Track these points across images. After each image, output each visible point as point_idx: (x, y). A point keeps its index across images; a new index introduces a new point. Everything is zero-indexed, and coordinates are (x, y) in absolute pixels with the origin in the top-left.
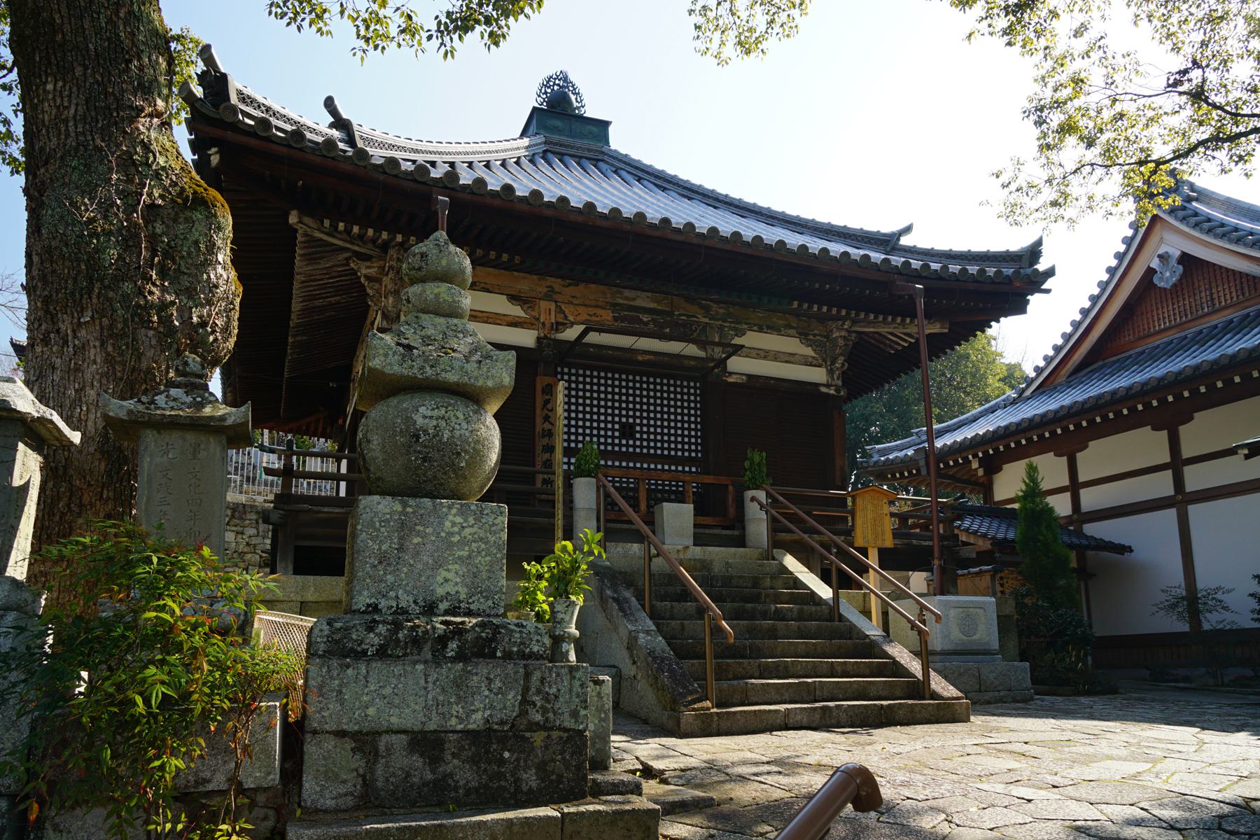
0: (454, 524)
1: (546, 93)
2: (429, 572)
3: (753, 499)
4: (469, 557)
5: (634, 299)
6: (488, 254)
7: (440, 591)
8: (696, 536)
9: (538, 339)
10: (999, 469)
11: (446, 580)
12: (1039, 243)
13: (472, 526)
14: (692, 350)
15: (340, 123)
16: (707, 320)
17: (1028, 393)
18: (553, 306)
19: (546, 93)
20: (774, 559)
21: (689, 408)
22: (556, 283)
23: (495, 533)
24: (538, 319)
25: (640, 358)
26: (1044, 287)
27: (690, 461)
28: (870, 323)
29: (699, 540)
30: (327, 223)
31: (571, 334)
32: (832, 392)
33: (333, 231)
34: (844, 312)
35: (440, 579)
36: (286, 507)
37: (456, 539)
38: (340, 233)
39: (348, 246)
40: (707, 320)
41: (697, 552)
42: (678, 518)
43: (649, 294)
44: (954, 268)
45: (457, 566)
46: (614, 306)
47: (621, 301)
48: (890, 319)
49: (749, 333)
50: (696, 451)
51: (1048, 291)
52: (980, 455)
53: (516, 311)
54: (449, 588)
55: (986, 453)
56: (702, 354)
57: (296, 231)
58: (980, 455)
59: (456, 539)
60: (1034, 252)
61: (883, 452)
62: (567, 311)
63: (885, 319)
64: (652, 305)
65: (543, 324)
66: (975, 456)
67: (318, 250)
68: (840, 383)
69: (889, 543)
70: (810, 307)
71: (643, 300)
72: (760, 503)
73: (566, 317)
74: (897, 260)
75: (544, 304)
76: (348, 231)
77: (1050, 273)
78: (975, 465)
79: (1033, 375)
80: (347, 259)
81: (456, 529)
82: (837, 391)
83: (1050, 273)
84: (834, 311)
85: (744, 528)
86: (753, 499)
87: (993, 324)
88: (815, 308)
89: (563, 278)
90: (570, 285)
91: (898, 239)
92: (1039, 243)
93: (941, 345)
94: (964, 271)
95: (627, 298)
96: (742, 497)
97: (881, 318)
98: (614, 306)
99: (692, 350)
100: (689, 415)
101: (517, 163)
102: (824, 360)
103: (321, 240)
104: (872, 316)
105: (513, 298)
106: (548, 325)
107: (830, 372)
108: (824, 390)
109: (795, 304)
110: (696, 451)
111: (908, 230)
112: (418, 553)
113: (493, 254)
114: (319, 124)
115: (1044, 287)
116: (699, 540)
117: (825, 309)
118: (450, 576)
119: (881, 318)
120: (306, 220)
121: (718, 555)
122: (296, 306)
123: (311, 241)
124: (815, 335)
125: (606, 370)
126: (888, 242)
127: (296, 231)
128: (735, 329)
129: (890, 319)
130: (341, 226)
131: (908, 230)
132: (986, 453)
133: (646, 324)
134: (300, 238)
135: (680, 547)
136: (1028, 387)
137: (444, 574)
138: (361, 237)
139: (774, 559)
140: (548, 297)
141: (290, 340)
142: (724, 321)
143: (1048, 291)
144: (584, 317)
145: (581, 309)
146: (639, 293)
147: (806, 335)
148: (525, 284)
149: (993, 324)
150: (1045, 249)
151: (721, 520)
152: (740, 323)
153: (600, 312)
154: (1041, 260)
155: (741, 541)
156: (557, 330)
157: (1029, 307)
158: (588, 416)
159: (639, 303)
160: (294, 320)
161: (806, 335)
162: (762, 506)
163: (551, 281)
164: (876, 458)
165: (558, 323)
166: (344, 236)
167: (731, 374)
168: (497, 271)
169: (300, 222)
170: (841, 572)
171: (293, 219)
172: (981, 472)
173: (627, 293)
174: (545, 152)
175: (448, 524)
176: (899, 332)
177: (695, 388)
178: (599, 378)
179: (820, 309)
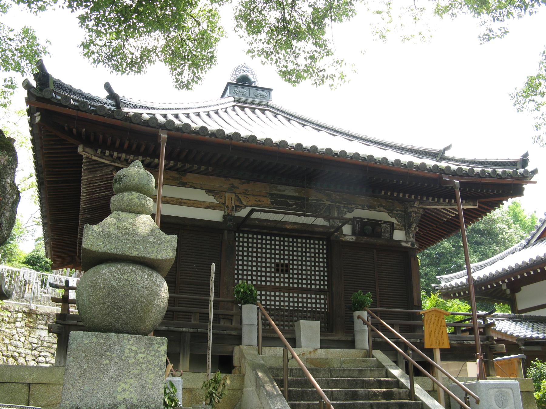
0: (131, 351)
1: (236, 74)
2: (112, 384)
3: (359, 317)
4: (140, 374)
5: (284, 191)
6: (177, 165)
7: (119, 398)
8: (322, 341)
9: (224, 216)
10: (519, 290)
11: (124, 390)
12: (527, 155)
13: (144, 353)
14: (320, 221)
15: (113, 96)
16: (329, 203)
17: (533, 241)
18: (233, 196)
19: (236, 74)
20: (373, 357)
21: (319, 258)
22: (236, 182)
23: (159, 357)
24: (224, 204)
25: (288, 227)
26: (531, 180)
27: (320, 291)
28: (430, 204)
29: (325, 344)
30: (99, 151)
31: (243, 213)
32: (409, 246)
33: (103, 156)
34: (413, 197)
35: (119, 389)
36: (64, 322)
37: (132, 361)
38: (107, 156)
39: (112, 164)
40: (329, 203)
41: (322, 353)
42: (310, 331)
43: (293, 188)
44: (477, 169)
45: (132, 380)
46: (271, 195)
47: (276, 192)
48: (442, 200)
49: (356, 210)
50: (324, 285)
51: (535, 182)
52: (506, 281)
53: (211, 199)
54: (126, 395)
55: (509, 280)
56: (326, 223)
57: (82, 156)
58: (506, 281)
59: (132, 361)
60: (524, 162)
61: (447, 280)
62: (242, 199)
63: (439, 200)
64: (294, 194)
65: (227, 207)
66: (503, 282)
67: (95, 166)
68: (414, 240)
69: (447, 346)
70: (392, 194)
71: (290, 191)
72: (363, 320)
73: (241, 203)
74: (443, 164)
75: (228, 195)
76: (111, 156)
77: (535, 172)
78: (504, 287)
79: (539, 224)
80: (112, 171)
81: (132, 355)
82: (413, 244)
83: (535, 172)
84: (407, 196)
85: (354, 336)
86: (359, 317)
87: (504, 202)
88: (395, 194)
89: (239, 178)
90: (244, 183)
91: (444, 153)
92: (527, 155)
93: (472, 216)
94: (494, 172)
95: (280, 190)
96: (352, 317)
97: (436, 200)
98: (271, 195)
99: (320, 221)
100: (319, 262)
101: (217, 113)
102: (404, 226)
103: (96, 161)
104: (431, 199)
105: (209, 191)
106: (230, 208)
107: (407, 233)
108: (404, 244)
109: (383, 193)
110: (324, 285)
111: (449, 148)
112: (106, 371)
113: (203, 168)
114: (103, 95)
115: (531, 180)
116: (325, 344)
117: (401, 195)
118: (126, 386)
119: (436, 200)
120: (88, 150)
121: (336, 355)
122: (83, 198)
123: (90, 161)
124: (397, 211)
125: (266, 235)
126: (438, 155)
127: (82, 156)
128: (348, 208)
129: (442, 200)
130: (107, 153)
131: (449, 148)
132: (509, 280)
133: (291, 206)
134: (84, 161)
135: (311, 350)
136: (538, 231)
137: (123, 385)
138: (119, 158)
139: (373, 357)
140: (230, 191)
141: (80, 217)
142: (341, 203)
143: (535, 182)
144: (253, 202)
145: (251, 197)
146: (287, 187)
147: (392, 210)
148: (217, 183)
149: (504, 202)
150: (530, 157)
151: (338, 331)
152: (350, 204)
153: (262, 199)
154: (529, 164)
155: (351, 344)
156: (236, 210)
157: (524, 192)
158: (295, 253)
159: (287, 193)
160: (82, 206)
161: (392, 210)
162: (364, 322)
163: (233, 181)
164: (443, 284)
165: (236, 206)
166: (110, 158)
167: (345, 235)
168: (199, 176)
169: (84, 151)
170: (415, 368)
171: (80, 150)
172: (508, 291)
173: (279, 187)
174: (234, 106)
175: (127, 351)
176: (446, 209)
177: (323, 245)
178: (262, 239)
179: (398, 195)
